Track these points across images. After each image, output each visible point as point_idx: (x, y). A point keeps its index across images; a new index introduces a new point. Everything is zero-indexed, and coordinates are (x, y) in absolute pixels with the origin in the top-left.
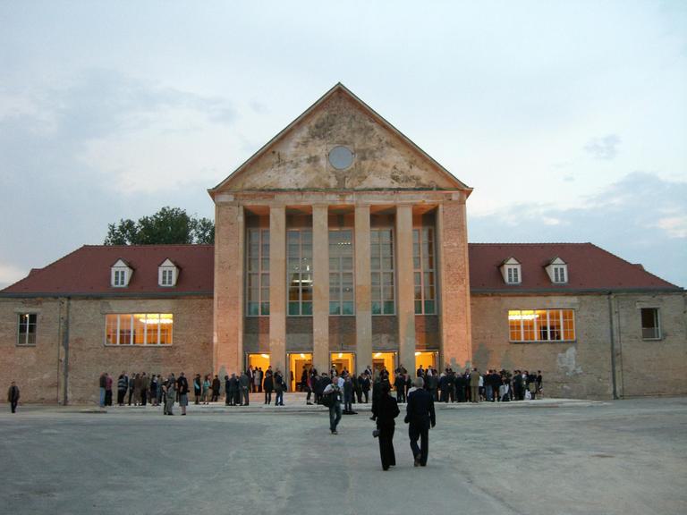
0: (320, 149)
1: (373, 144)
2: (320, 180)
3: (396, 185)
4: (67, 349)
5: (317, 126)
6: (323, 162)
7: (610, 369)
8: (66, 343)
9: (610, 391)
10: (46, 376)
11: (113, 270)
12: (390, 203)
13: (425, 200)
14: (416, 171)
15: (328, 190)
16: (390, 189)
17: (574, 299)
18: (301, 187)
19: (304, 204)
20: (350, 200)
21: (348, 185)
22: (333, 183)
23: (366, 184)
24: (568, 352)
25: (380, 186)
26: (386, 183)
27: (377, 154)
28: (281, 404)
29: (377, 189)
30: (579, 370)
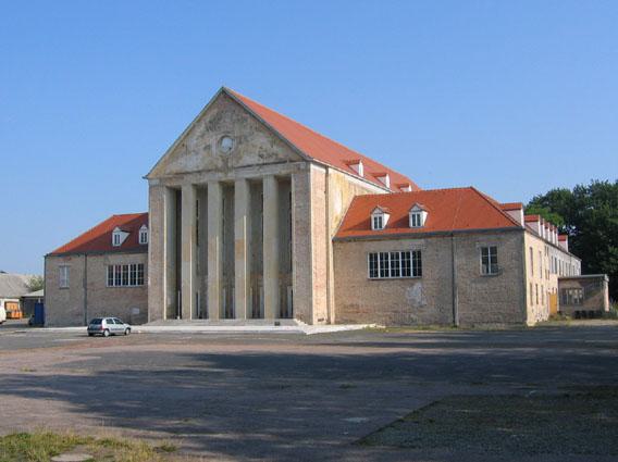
0: (212, 139)
1: (246, 131)
2: (212, 162)
3: (261, 162)
4: (86, 289)
5: (210, 122)
6: (214, 149)
7: (451, 301)
8: (85, 285)
9: (450, 320)
10: (75, 308)
11: (114, 234)
12: (257, 175)
13: (281, 170)
14: (275, 149)
15: (217, 170)
16: (258, 165)
17: (423, 240)
18: (200, 168)
19: (202, 181)
20: (231, 176)
21: (229, 165)
22: (220, 164)
23: (241, 163)
24: (415, 288)
25: (250, 163)
26: (255, 160)
27: (249, 139)
28: (485, 251)
29: (249, 166)
30: (424, 302)
